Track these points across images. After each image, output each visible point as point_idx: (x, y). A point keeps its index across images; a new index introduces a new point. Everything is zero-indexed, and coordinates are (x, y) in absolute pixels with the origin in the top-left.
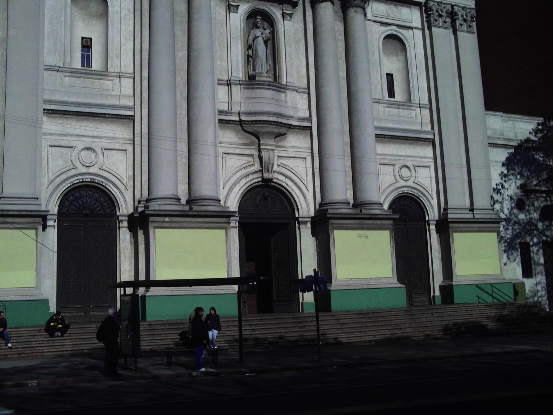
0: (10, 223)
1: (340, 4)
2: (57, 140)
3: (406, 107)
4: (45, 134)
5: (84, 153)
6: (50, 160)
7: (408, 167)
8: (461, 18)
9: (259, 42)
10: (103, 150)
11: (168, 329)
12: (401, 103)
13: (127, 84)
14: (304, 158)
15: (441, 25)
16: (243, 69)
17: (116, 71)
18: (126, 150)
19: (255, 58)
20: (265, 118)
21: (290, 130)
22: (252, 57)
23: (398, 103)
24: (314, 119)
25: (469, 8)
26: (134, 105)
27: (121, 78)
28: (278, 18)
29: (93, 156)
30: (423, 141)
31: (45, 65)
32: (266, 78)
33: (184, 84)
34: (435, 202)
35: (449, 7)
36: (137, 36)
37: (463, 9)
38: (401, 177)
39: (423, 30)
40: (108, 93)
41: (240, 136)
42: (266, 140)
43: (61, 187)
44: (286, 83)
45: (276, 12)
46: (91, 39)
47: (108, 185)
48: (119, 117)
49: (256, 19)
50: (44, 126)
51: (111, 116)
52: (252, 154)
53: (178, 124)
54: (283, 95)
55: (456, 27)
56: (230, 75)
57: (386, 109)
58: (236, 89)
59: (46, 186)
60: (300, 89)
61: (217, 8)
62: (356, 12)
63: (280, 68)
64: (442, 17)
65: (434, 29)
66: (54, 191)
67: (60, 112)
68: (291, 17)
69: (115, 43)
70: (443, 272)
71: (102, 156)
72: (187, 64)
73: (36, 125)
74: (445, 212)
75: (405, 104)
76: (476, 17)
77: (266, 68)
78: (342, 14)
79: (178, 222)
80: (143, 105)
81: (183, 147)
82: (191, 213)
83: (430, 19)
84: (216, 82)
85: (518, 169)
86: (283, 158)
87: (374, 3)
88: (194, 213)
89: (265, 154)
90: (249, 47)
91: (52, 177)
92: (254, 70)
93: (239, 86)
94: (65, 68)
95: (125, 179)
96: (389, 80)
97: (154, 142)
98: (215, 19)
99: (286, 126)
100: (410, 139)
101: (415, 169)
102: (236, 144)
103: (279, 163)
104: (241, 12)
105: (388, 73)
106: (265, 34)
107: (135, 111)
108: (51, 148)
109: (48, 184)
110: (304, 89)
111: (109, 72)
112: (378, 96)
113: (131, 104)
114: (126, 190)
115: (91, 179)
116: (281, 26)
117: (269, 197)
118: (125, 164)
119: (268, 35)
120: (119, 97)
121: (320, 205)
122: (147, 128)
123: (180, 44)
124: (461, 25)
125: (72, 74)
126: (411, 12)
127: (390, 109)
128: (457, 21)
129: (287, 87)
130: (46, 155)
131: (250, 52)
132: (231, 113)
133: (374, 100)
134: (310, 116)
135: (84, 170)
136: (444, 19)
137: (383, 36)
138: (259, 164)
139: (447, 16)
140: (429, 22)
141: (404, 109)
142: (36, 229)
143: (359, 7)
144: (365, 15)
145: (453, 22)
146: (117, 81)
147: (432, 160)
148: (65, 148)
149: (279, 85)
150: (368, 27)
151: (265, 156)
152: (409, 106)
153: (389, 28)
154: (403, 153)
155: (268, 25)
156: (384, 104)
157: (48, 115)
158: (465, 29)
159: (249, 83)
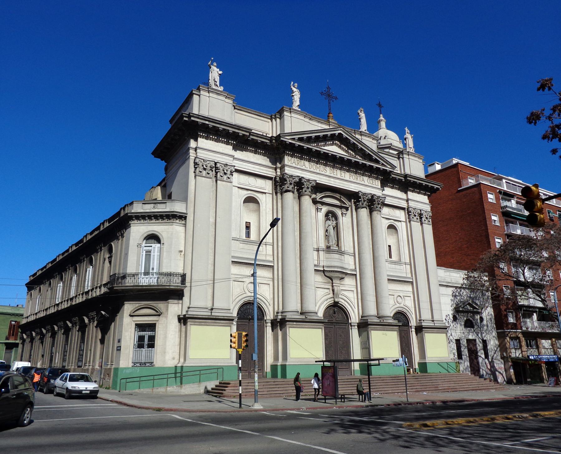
20: (336, 269)
24: (358, 270)
34: (414, 316)
38: (398, 302)
39: (406, 222)
41: (323, 278)
44: (189, 308)
45: (338, 212)
58: (321, 253)
63: (341, 242)
66: (236, 305)
79: (218, 323)
82: (307, 320)
85: (525, 242)
88: (308, 320)
89: (335, 288)
90: (327, 231)
92: (148, 253)
102: (321, 282)
112: (234, 234)
117: (349, 282)
121: (362, 317)
124: (425, 220)
132: (320, 266)
134: (356, 268)
145: (421, 218)
154: (398, 289)
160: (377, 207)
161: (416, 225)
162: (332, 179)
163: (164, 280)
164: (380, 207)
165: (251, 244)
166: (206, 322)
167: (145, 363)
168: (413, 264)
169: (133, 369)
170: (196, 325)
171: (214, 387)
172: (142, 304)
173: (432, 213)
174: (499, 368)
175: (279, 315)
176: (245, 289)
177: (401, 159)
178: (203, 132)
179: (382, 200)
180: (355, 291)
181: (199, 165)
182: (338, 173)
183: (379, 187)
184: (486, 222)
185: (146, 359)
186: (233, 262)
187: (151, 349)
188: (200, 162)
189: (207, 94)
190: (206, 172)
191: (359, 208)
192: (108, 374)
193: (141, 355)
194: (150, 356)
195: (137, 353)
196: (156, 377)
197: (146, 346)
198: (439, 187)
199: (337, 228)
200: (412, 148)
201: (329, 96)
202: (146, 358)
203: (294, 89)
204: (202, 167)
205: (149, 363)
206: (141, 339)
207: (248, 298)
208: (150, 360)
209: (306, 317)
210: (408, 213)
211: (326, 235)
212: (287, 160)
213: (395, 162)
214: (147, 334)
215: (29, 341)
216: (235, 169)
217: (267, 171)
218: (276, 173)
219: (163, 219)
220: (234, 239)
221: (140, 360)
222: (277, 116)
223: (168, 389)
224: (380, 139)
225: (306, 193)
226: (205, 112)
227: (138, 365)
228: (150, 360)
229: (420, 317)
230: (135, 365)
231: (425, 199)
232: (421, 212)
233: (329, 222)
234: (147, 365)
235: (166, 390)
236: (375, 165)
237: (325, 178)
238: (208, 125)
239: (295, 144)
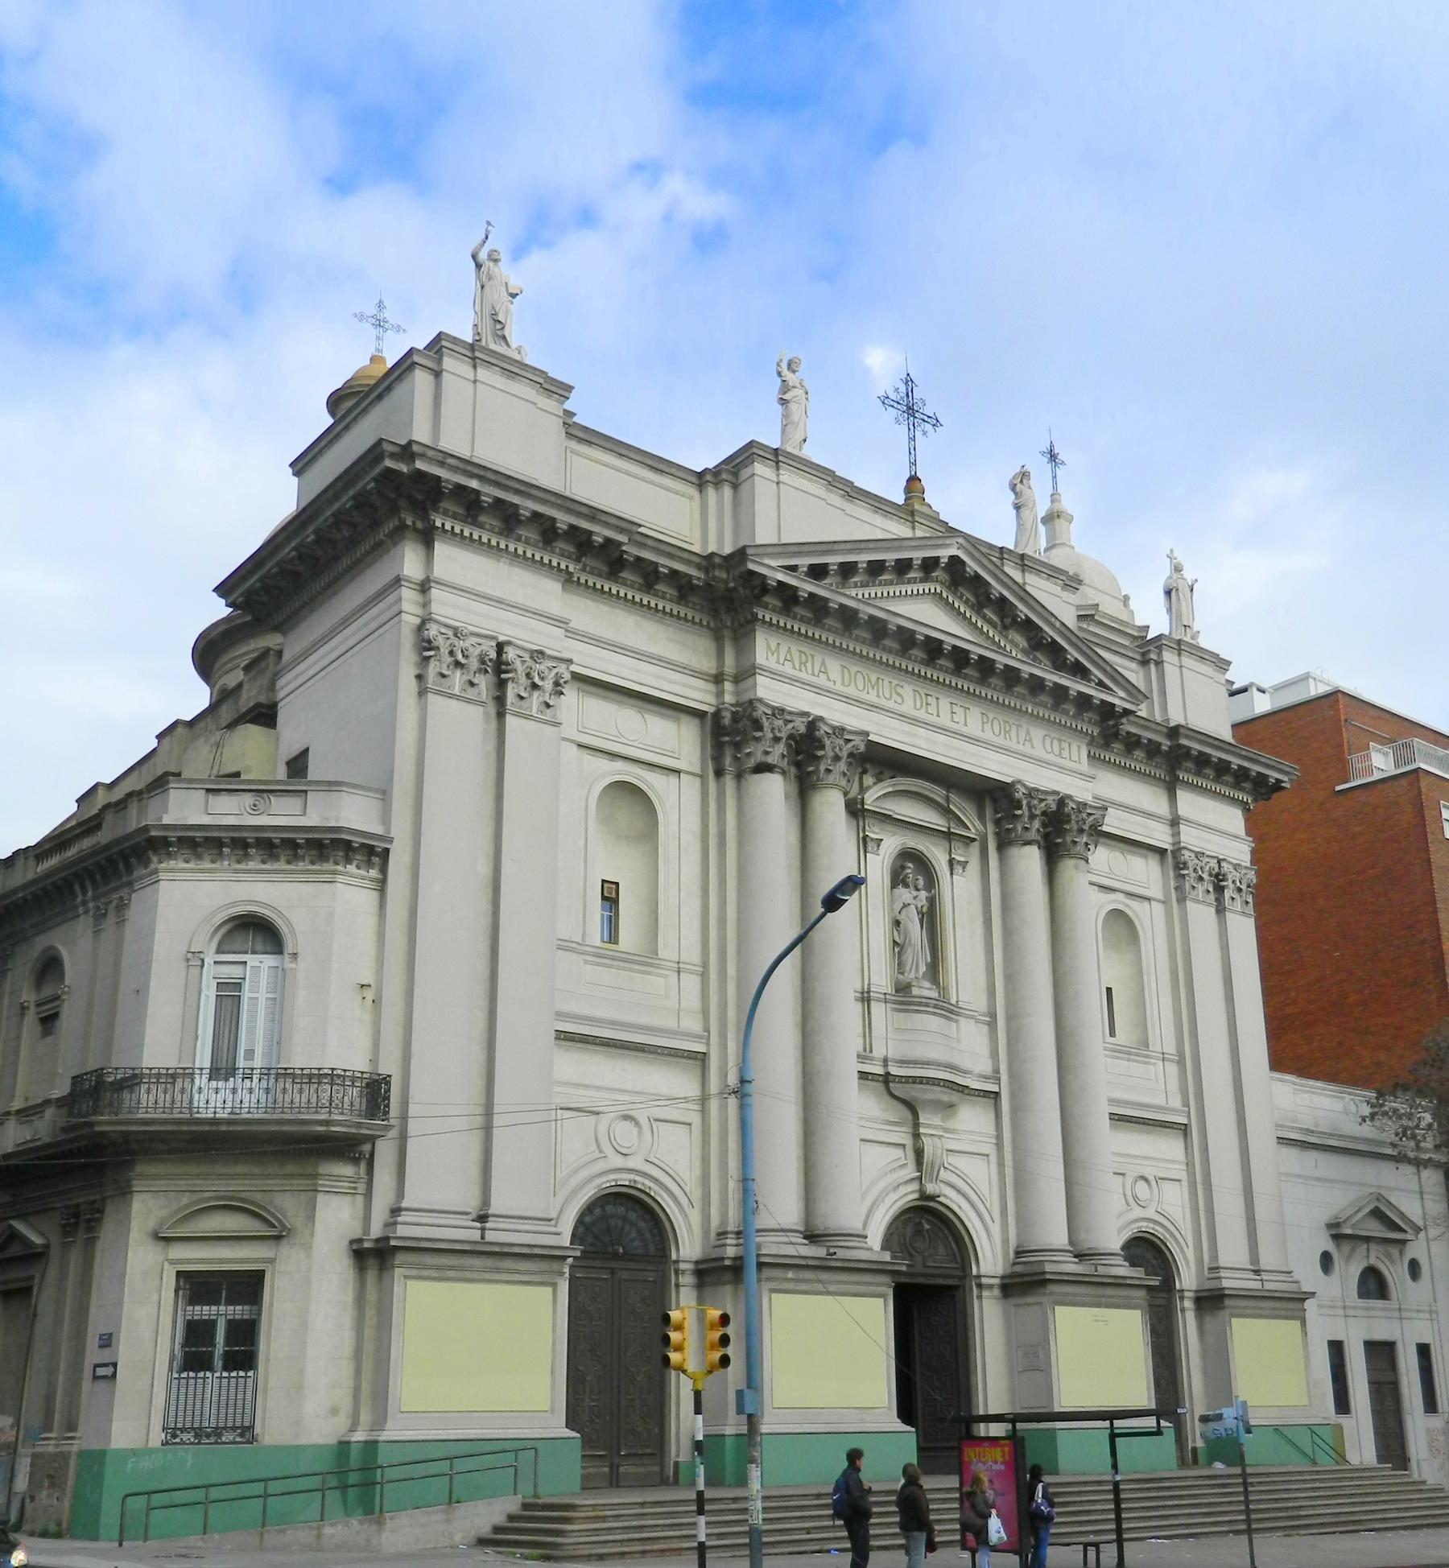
0: (431, 1267)
11: (638, 1515)
14: (985, 1155)
24: (1004, 1078)
29: (635, 1131)
34: (1190, 1253)
35: (1213, 863)
38: (1135, 1198)
42: (928, 1116)
44: (396, 1211)
45: (938, 855)
47: (659, 1195)
52: (903, 1142)
70: (149, 987)
74: (392, 1220)
82: (834, 1264)
88: (839, 1264)
90: (897, 923)
92: (230, 995)
94: (705, 964)
112: (567, 929)
115: (630, 1181)
117: (973, 1120)
125: (599, 960)
132: (872, 1059)
134: (997, 1071)
135: (619, 1162)
137: (1114, 906)
142: (554, 1285)
145: (1219, 890)
152: (1147, 1056)
161: (1201, 913)
162: (921, 731)
163: (254, 1100)
164: (1087, 844)
165: (625, 969)
166: (462, 1269)
167: (218, 1432)
168: (1188, 1061)
169: (170, 1456)
170: (448, 1279)
171: (500, 1519)
172: (207, 1195)
173: (1258, 874)
175: (728, 1241)
176: (602, 1144)
177: (1152, 666)
179: (1092, 818)
180: (993, 1158)
181: (437, 648)
182: (945, 709)
184: (1435, 912)
185: (222, 1415)
186: (563, 1037)
187: (242, 1373)
188: (518, 662)
190: (465, 678)
191: (1011, 843)
192: (50, 1477)
193: (199, 1397)
194: (240, 1402)
195: (183, 1390)
196: (273, 1487)
197: (218, 1362)
198: (1286, 779)
199: (931, 918)
201: (911, 410)
202: (223, 1411)
204: (450, 660)
205: (234, 1428)
206: (197, 1334)
208: (239, 1417)
209: (832, 1250)
211: (895, 942)
212: (767, 649)
213: (1133, 673)
214: (222, 1314)
217: (685, 685)
218: (720, 694)
219: (294, 858)
220: (564, 946)
221: (197, 1418)
223: (328, 1531)
227: (188, 1437)
228: (239, 1417)
229: (1214, 1255)
230: (174, 1436)
231: (1232, 819)
232: (1220, 867)
233: (905, 895)
234: (228, 1437)
235: (319, 1536)
236: (1076, 686)
237: (895, 723)
238: (478, 493)
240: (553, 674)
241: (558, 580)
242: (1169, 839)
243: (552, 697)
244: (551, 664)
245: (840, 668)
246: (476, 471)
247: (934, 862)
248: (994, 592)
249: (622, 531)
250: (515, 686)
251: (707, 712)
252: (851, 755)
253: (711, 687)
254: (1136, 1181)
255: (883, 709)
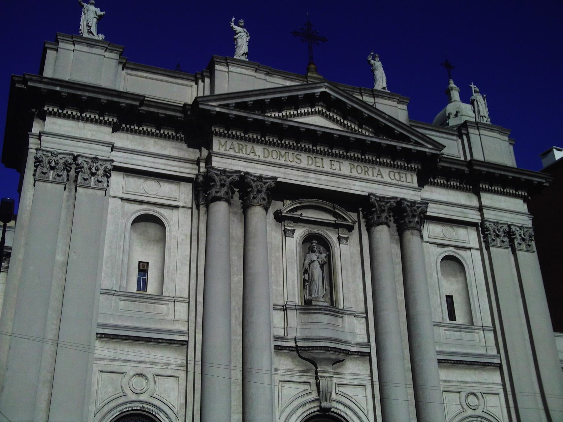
1: (396, 226)
2: (109, 365)
3: (468, 330)
4: (96, 359)
5: (135, 379)
6: (100, 386)
7: (475, 395)
8: (519, 237)
9: (315, 266)
10: (155, 376)
12: (462, 326)
13: (182, 308)
15: (499, 245)
16: (299, 293)
17: (171, 295)
18: (178, 377)
19: (311, 282)
20: (322, 344)
21: (348, 356)
22: (308, 281)
23: (460, 326)
24: (373, 344)
25: (526, 228)
26: (188, 330)
27: (176, 303)
28: (334, 242)
29: (144, 382)
30: (489, 366)
31: (101, 289)
32: (323, 302)
33: (239, 309)
35: (505, 227)
36: (193, 261)
37: (520, 229)
38: (469, 406)
39: (481, 250)
40: (162, 317)
42: (323, 367)
43: (109, 416)
44: (343, 307)
45: (332, 236)
46: (147, 263)
47: (158, 414)
48: (172, 342)
49: (312, 243)
50: (96, 352)
51: (164, 341)
53: (232, 350)
54: (340, 320)
55: (515, 246)
56: (286, 300)
57: (447, 332)
58: (292, 314)
59: (93, 415)
60: (357, 313)
61: (273, 233)
62: (412, 234)
63: (337, 292)
64: (500, 237)
65: (492, 249)
67: (114, 337)
68: (347, 241)
69: (171, 268)
71: (153, 383)
72: (242, 288)
73: (88, 350)
75: (467, 326)
76: (534, 236)
77: (322, 292)
78: (398, 237)
80: (197, 330)
81: (238, 375)
83: (488, 239)
84: (272, 307)
86: (341, 386)
87: (430, 225)
89: (322, 382)
90: (305, 271)
91: (101, 405)
92: (310, 295)
93: (295, 311)
94: (121, 292)
95: (176, 408)
96: (449, 302)
97: (207, 369)
98: (271, 244)
99: (344, 352)
100: (475, 363)
101: (483, 397)
103: (338, 391)
104: (297, 236)
105: (448, 294)
106: (321, 258)
107: (188, 336)
108: (101, 373)
109: (96, 412)
110: (362, 313)
111: (164, 296)
112: (438, 319)
113: (185, 329)
114: (177, 419)
115: (141, 407)
116: (337, 250)
118: (177, 391)
119: (324, 259)
120: (173, 321)
122: (200, 354)
123: (235, 269)
125: (450, 329)
126: (468, 233)
127: (452, 332)
128: (515, 240)
129: (345, 312)
130: (96, 381)
131: (306, 276)
132: (287, 339)
133: (435, 323)
134: (369, 341)
135: (134, 397)
136: (502, 239)
137: (441, 257)
138: (317, 392)
139: (504, 236)
140: (486, 242)
141: (466, 332)
143: (415, 229)
144: (422, 237)
145: (512, 241)
146: (171, 305)
147: (501, 387)
148: (115, 374)
149: (337, 310)
150: (425, 250)
151: (323, 384)
152: (472, 329)
153: (446, 249)
154: (469, 379)
155: (324, 249)
156: (445, 327)
157: (101, 339)
158: (525, 249)
159: (305, 307)
160: (410, 222)
162: (312, 175)
174: (56, 123)
178: (221, 125)
179: (420, 209)
183: (416, 184)
188: (85, 163)
189: (71, 47)
198: (544, 181)
200: (487, 116)
203: (238, 29)
207: (131, 405)
210: (483, 232)
215: (248, 40)
216: (114, 166)
217: (180, 167)
221: (61, 345)
222: (204, 74)
224: (449, 117)
225: (255, 201)
226: (545, 166)
231: (520, 205)
237: (295, 172)
239: (246, 118)
240: (103, 167)
241: (522, 199)
242: (480, 218)
243: (103, 177)
244: (102, 163)
245: (306, 158)
246: (58, 83)
247: (329, 239)
248: (348, 105)
249: (135, 100)
250: (82, 174)
251: (478, 223)
252: (267, 189)
253: (196, 167)
254: (468, 396)
255: (356, 178)
